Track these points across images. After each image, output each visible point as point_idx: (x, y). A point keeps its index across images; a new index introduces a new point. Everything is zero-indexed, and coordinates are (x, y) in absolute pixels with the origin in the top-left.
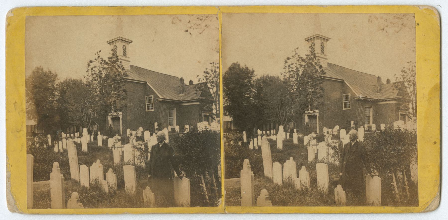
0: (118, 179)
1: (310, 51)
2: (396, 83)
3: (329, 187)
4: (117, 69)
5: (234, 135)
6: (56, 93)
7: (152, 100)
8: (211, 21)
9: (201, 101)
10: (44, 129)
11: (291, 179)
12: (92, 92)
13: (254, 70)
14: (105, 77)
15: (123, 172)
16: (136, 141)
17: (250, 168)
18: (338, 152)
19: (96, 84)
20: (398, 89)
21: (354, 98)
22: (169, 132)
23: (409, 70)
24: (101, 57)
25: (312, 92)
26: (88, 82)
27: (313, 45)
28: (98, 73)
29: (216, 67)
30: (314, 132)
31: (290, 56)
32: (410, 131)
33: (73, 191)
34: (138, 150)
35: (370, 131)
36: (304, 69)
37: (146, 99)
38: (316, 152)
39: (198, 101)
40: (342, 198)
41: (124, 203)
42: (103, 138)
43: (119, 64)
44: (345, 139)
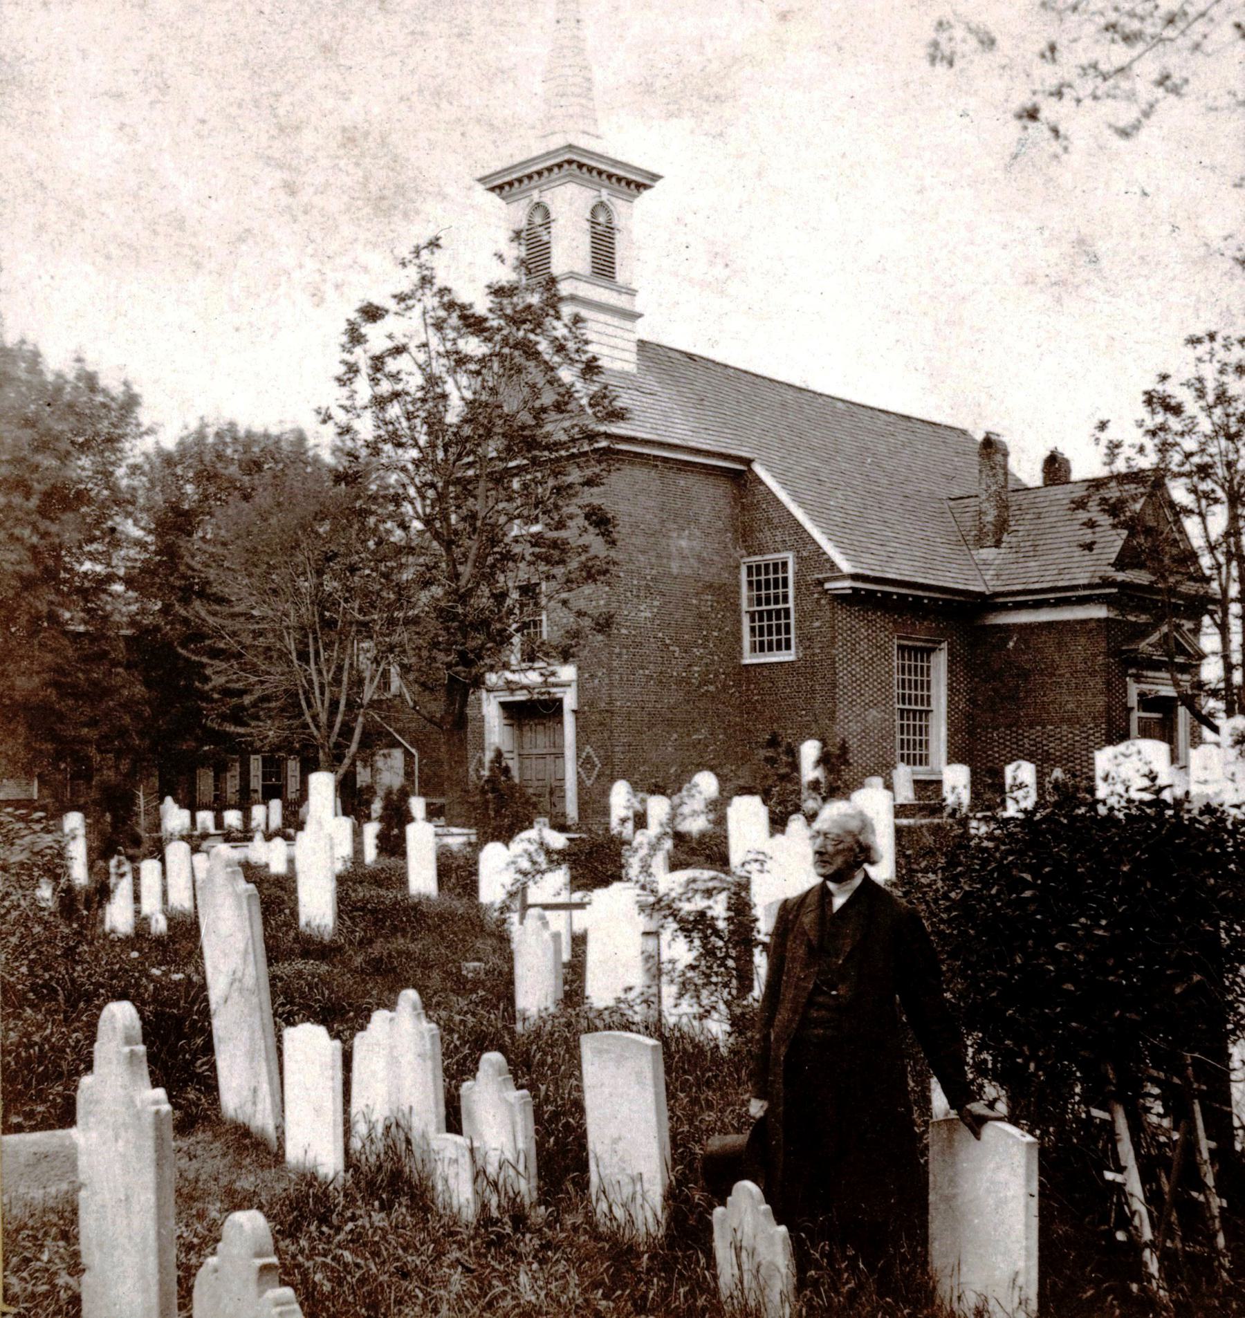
1: (523, 262)
2: (1112, 477)
4: (552, 369)
6: (131, 529)
10: (40, 776)
11: (408, 1142)
12: (372, 520)
13: (136, 389)
14: (466, 421)
16: (674, 866)
19: (404, 469)
21: (820, 583)
23: (1201, 394)
24: (439, 283)
25: (533, 546)
26: (349, 454)
27: (538, 220)
28: (420, 394)
29: (1230, 369)
31: (381, 298)
33: (237, 1201)
34: (682, 929)
41: (585, 1291)
43: (565, 331)
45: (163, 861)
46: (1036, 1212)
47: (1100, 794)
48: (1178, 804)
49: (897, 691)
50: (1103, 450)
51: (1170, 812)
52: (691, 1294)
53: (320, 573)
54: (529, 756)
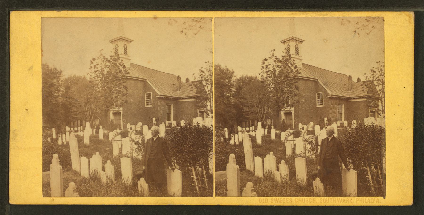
0: (116, 170)
1: (286, 52)
4: (119, 67)
7: (322, 96)
8: (205, 22)
9: (197, 98)
12: (94, 88)
13: (234, 70)
14: (278, 74)
15: (295, 164)
16: (135, 134)
18: (141, 147)
19: (270, 81)
20: (367, 88)
21: (156, 96)
22: (338, 127)
23: (207, 70)
24: (275, 56)
26: (91, 79)
27: (288, 47)
30: (118, 128)
31: (267, 58)
32: (208, 127)
36: (108, 69)
38: (120, 147)
39: (194, 98)
40: (144, 190)
41: (296, 193)
42: (277, 131)
43: (292, 62)
44: (148, 135)
45: (238, 134)
46: (357, 181)
47: (365, 125)
48: (376, 126)
49: (338, 111)
50: (194, 78)
51: (375, 127)
52: (310, 193)
53: (87, 95)
54: (288, 120)
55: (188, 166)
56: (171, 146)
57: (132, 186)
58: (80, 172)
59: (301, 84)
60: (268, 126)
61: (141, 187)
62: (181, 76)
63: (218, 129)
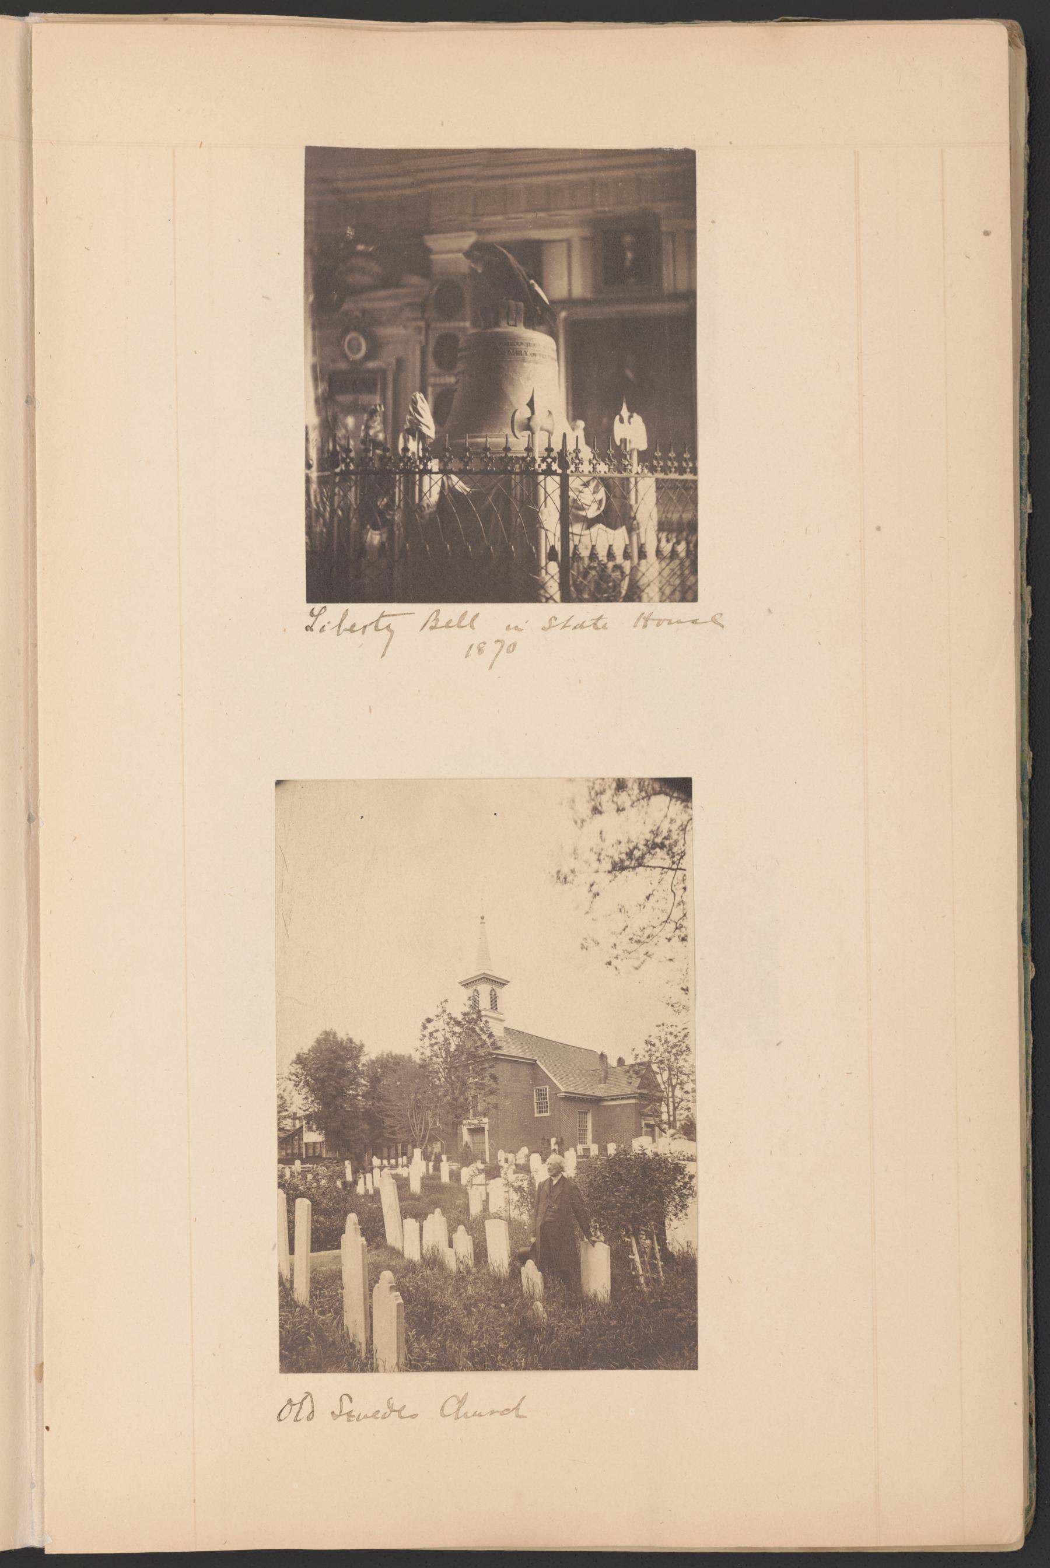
2: (635, 1064)
3: (510, 1264)
5: (327, 1168)
11: (438, 1251)
12: (430, 1078)
14: (455, 1050)
16: (515, 1172)
17: (359, 1231)
19: (439, 1064)
21: (556, 1094)
23: (660, 1040)
24: (448, 1012)
27: (475, 994)
30: (479, 1159)
35: (588, 1157)
36: (459, 1040)
37: (535, 1093)
38: (484, 1198)
44: (541, 1173)
53: (416, 1093)
55: (624, 1235)
56: (588, 1196)
57: (511, 1277)
58: (403, 1251)
59: (502, 1071)
60: (436, 1155)
61: (528, 1278)
62: (606, 1053)
63: (330, 1163)
